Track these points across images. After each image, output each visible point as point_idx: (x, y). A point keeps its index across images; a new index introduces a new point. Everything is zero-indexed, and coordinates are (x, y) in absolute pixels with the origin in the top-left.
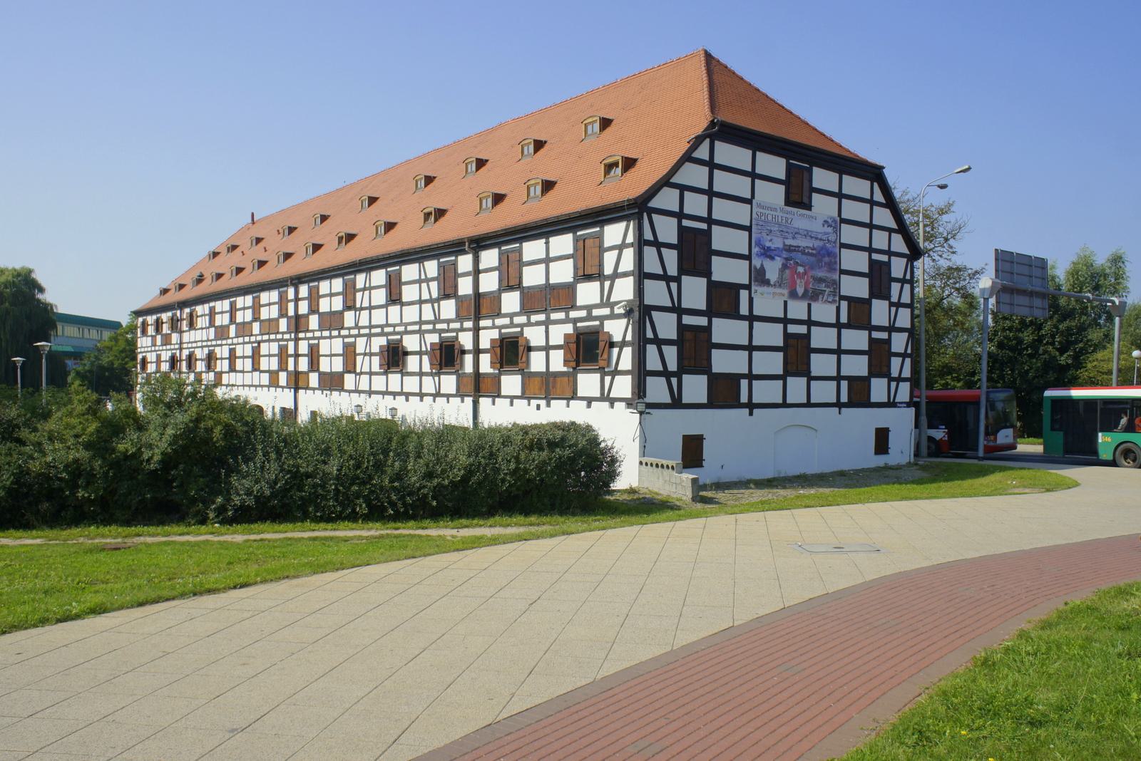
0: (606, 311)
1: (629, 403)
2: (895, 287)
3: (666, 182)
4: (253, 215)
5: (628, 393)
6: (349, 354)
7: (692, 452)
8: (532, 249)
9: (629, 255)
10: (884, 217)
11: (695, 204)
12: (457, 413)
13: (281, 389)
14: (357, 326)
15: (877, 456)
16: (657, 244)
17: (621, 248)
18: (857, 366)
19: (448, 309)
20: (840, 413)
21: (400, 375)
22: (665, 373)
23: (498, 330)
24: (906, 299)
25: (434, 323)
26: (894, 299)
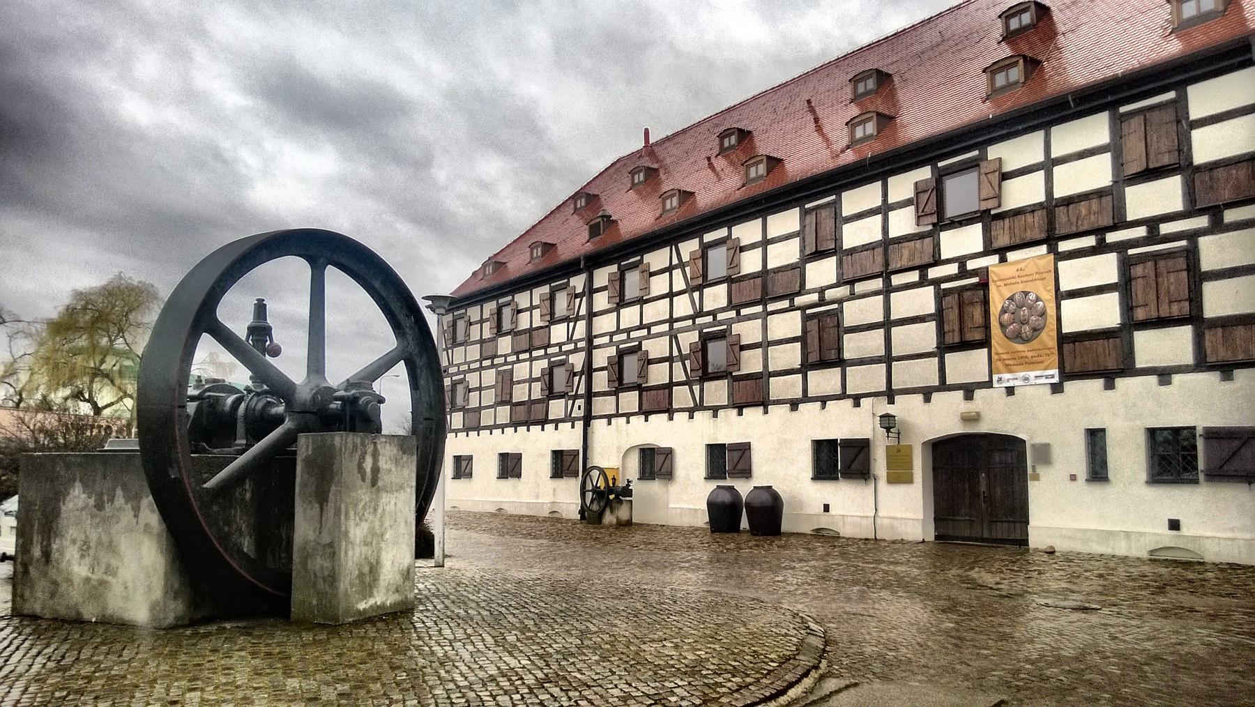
0: (571, 347)
4: (647, 133)
8: (857, 199)
15: (1141, 440)
25: (693, 318)
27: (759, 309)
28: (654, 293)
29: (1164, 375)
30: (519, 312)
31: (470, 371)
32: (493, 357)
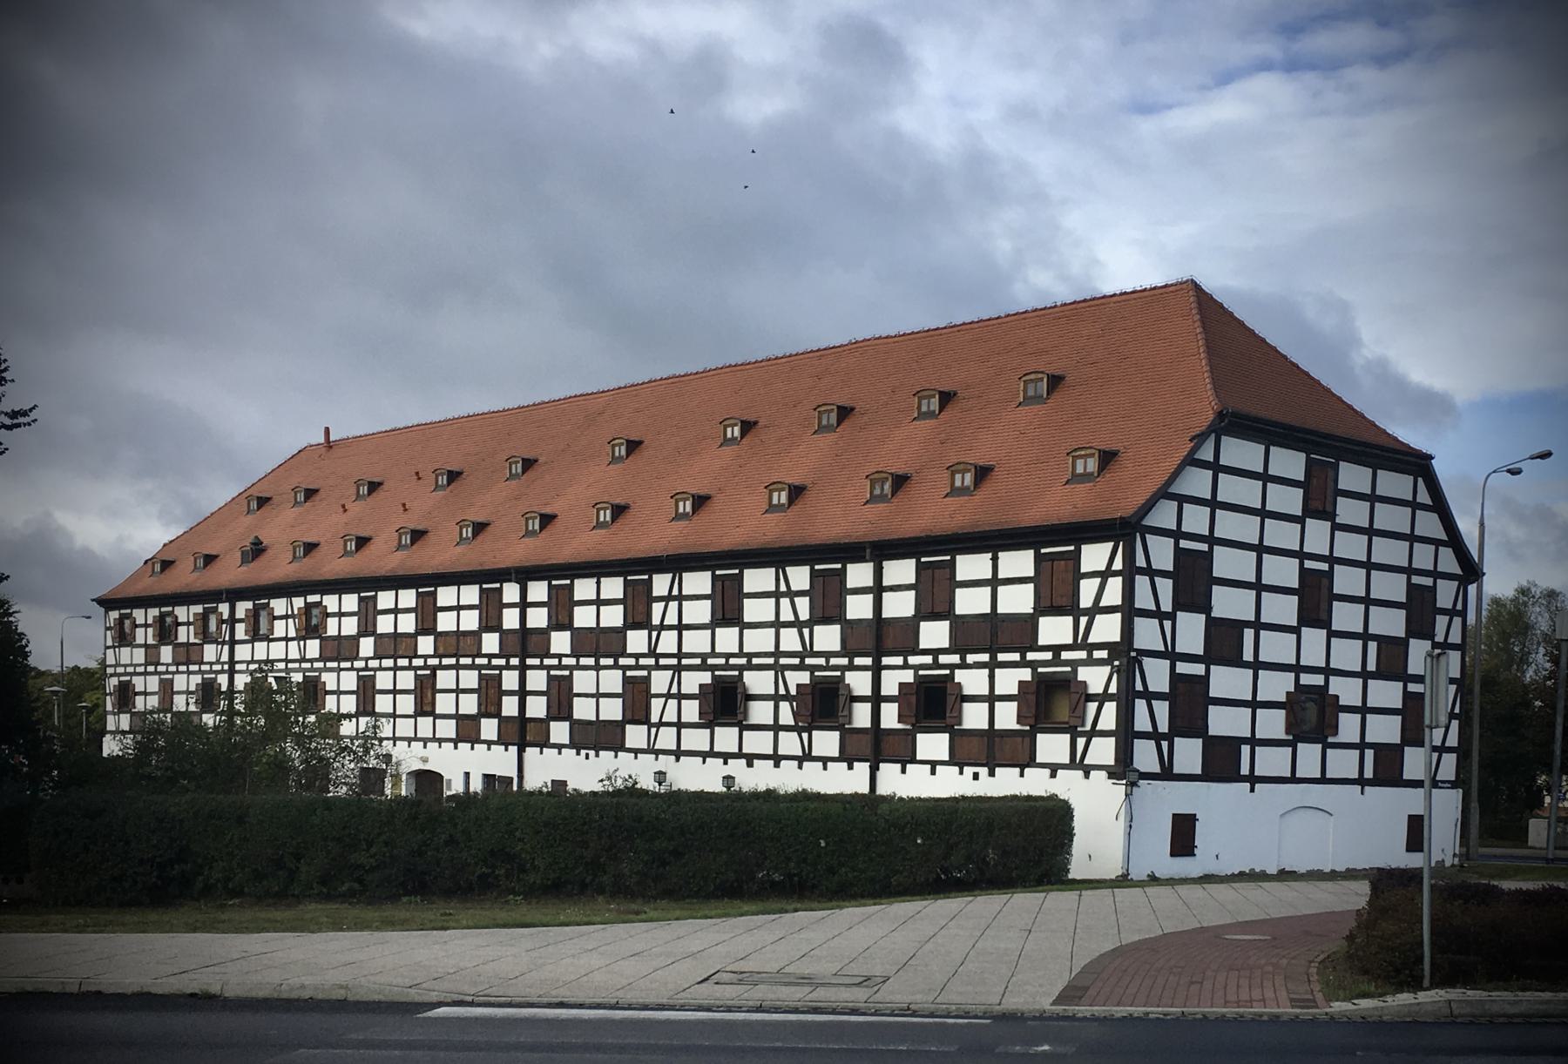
1: (1113, 774)
2: (1441, 622)
3: (1164, 493)
5: (1110, 760)
6: (637, 699)
7: (1183, 835)
9: (1115, 586)
10: (1429, 525)
11: (1196, 520)
12: (850, 780)
13: (485, 746)
14: (652, 653)
16: (1151, 572)
17: (1105, 575)
18: (1386, 730)
19: (828, 637)
20: (1362, 793)
21: (736, 729)
22: (1155, 735)
23: (912, 671)
24: (1455, 637)
25: (801, 656)
26: (1440, 638)
27: (684, 662)
28: (276, 635)
29: (933, 765)
30: (137, 626)
31: (136, 674)
32: (158, 664)
